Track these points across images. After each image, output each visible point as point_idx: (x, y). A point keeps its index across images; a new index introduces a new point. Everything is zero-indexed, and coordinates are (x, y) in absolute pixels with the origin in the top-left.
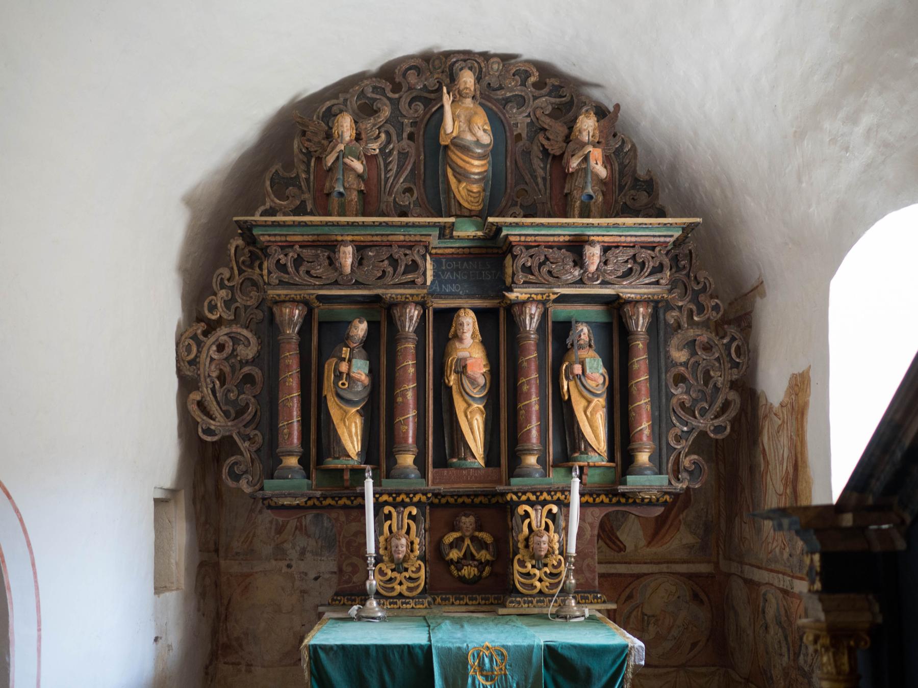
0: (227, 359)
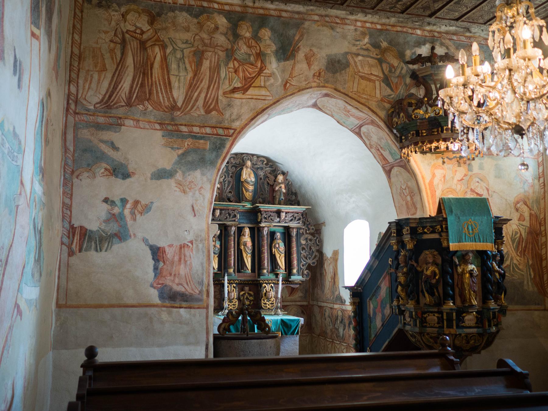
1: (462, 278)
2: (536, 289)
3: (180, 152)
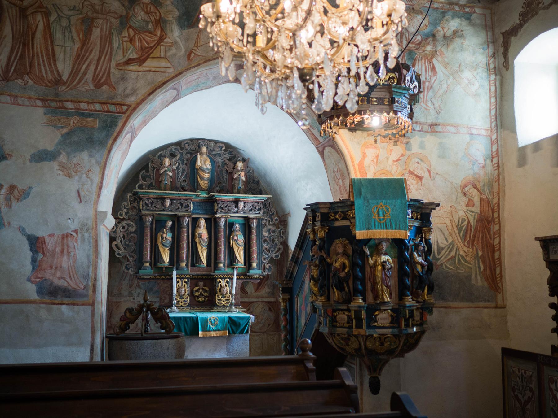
0: (126, 231)
1: (374, 271)
2: (486, 284)
3: (65, 131)
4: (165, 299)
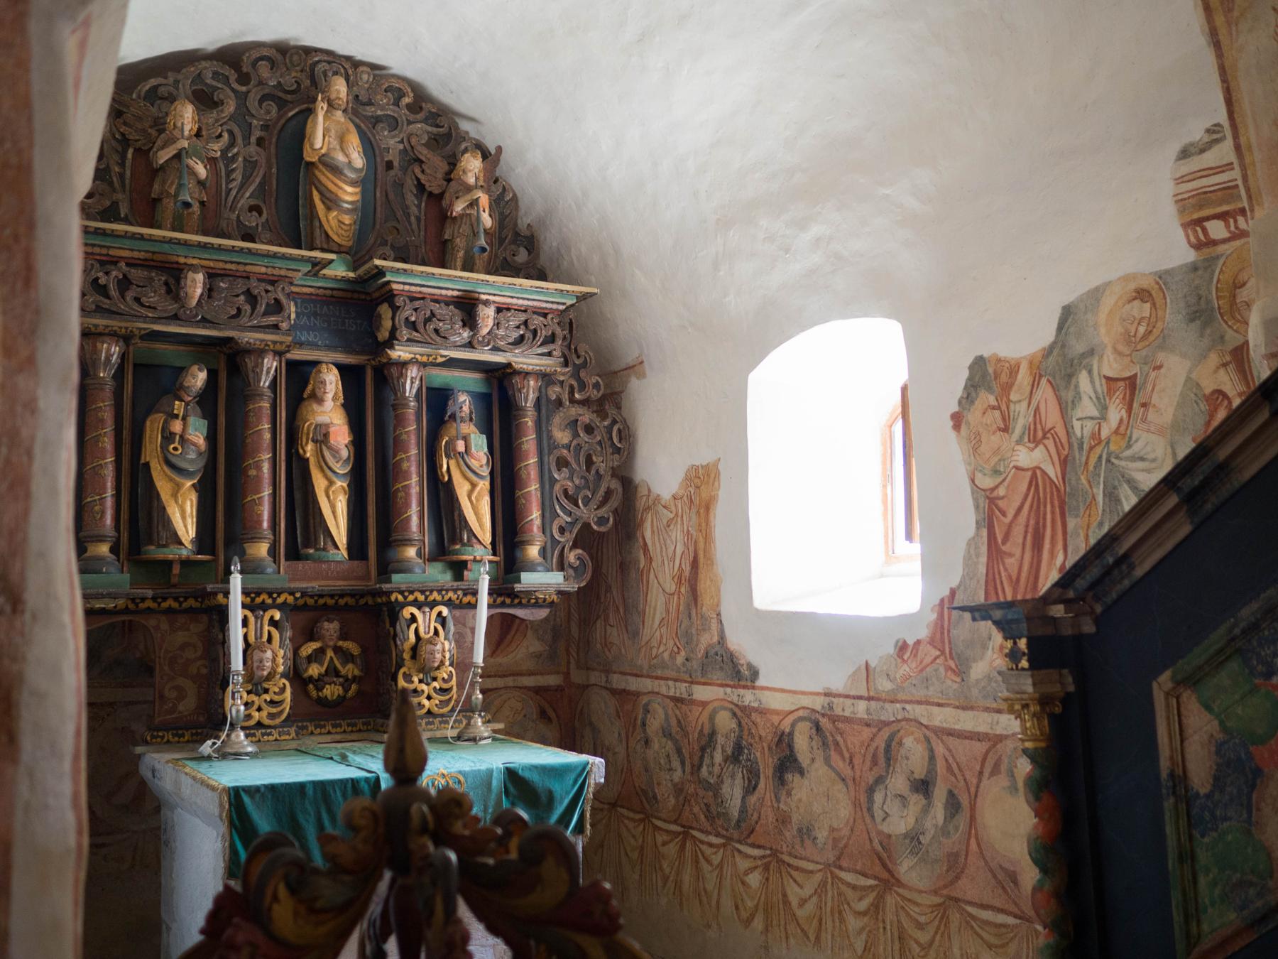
4: (181, 697)
